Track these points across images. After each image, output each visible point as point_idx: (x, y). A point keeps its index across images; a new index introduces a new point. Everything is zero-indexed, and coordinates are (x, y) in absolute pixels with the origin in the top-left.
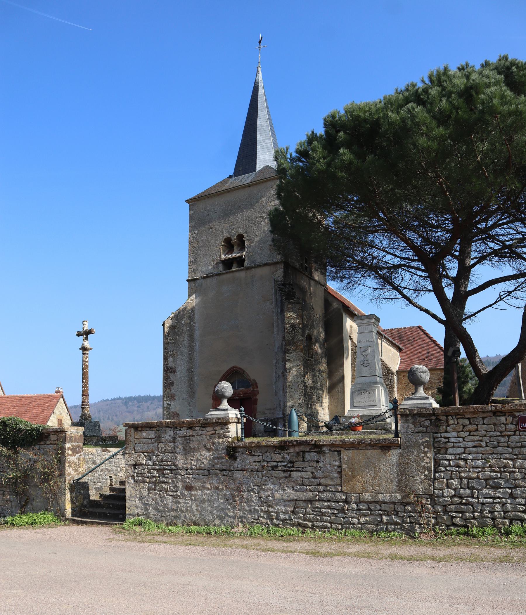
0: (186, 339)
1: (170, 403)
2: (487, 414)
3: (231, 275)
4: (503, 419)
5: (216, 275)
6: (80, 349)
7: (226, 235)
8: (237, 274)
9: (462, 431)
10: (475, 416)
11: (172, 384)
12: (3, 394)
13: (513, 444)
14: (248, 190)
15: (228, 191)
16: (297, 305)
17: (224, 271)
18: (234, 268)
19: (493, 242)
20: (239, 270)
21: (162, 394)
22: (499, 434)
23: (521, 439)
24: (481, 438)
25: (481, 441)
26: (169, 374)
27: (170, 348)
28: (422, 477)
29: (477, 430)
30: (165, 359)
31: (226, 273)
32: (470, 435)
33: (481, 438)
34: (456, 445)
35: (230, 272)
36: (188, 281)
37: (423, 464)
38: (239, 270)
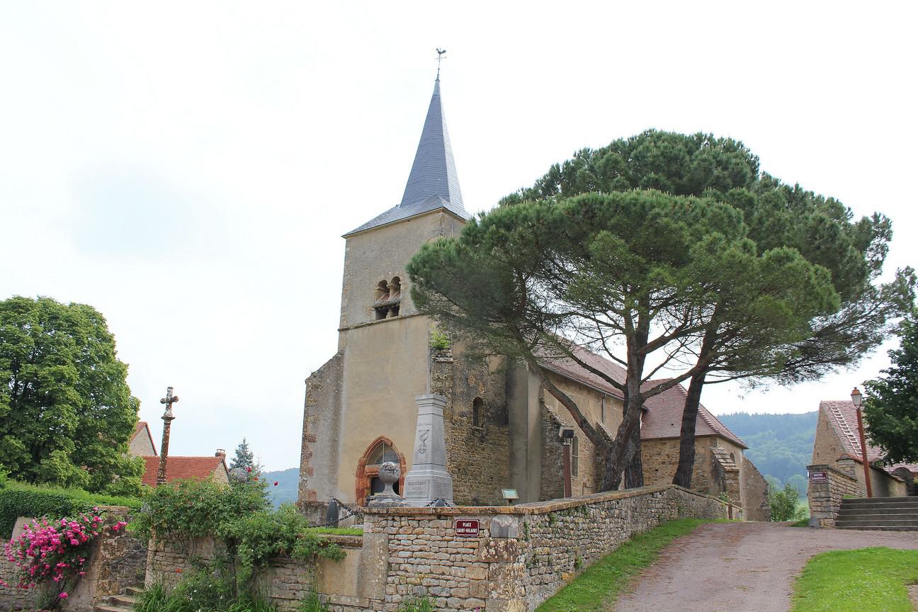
0: (331, 400)
1: (306, 479)
2: (433, 517)
3: (384, 324)
4: (443, 523)
5: (369, 325)
6: (162, 418)
7: (381, 278)
8: (391, 325)
9: (412, 534)
10: (422, 518)
11: (311, 455)
12: (153, 455)
13: (450, 550)
14: (407, 225)
15: (387, 226)
16: (448, 365)
17: (378, 321)
18: (388, 317)
19: (604, 312)
20: (393, 320)
21: (298, 466)
22: (440, 538)
23: (457, 544)
24: (425, 542)
25: (426, 545)
26: (307, 443)
27: (310, 412)
28: (377, 581)
29: (423, 533)
30: (305, 426)
31: (379, 323)
32: (417, 538)
33: (425, 542)
34: (405, 548)
35: (383, 322)
36: (338, 330)
37: (378, 566)
38: (393, 320)
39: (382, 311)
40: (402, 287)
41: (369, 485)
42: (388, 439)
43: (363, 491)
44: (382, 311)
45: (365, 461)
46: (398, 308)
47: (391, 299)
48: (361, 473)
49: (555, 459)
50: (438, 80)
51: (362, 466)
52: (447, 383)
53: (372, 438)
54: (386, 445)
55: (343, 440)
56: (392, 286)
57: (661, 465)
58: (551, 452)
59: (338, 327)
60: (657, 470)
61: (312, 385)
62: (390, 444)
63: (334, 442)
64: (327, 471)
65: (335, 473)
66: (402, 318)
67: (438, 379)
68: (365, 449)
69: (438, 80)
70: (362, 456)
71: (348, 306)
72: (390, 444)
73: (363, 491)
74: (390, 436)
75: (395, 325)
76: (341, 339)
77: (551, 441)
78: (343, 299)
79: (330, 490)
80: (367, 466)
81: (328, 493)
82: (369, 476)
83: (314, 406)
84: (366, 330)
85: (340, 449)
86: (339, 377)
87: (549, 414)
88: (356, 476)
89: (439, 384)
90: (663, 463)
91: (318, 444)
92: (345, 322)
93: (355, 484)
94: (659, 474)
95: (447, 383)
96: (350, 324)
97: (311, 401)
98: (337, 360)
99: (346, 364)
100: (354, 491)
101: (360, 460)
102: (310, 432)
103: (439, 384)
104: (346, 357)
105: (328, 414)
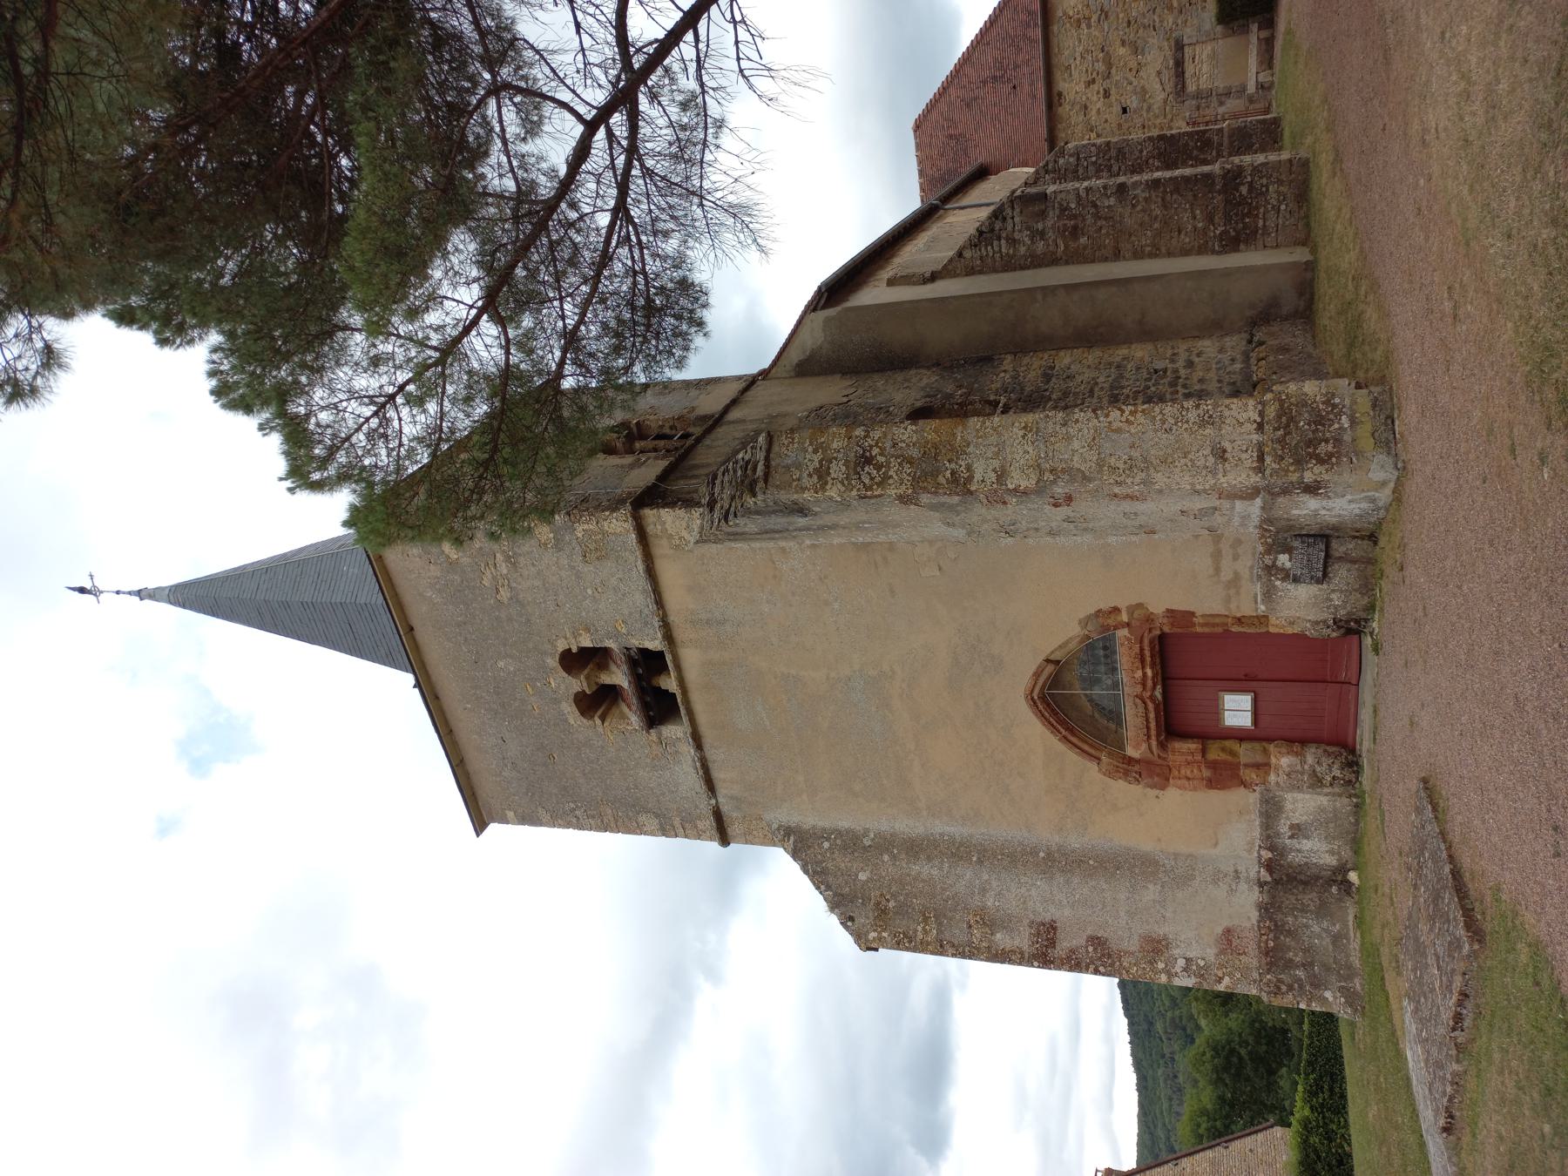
0: (923, 869)
1: (1181, 962)
16: (776, 448)
17: (685, 719)
18: (669, 683)
20: (678, 667)
39: (660, 708)
40: (587, 643)
41: (1192, 746)
42: (1037, 675)
43: (1213, 765)
44: (660, 708)
45: (1110, 755)
46: (644, 652)
47: (619, 677)
48: (1154, 773)
49: (1097, 217)
50: (141, 594)
51: (1128, 768)
52: (835, 445)
53: (1034, 732)
54: (1055, 681)
55: (1045, 835)
56: (587, 678)
57: (1113, 98)
58: (1075, 232)
59: (714, 846)
60: (1125, 110)
61: (874, 927)
62: (1050, 668)
63: (1054, 862)
64: (1151, 892)
65: (1156, 863)
66: (669, 637)
67: (822, 473)
68: (1072, 757)
69: (141, 594)
70: (1093, 766)
71: (657, 816)
72: (1050, 668)
73: (1213, 765)
74: (1022, 668)
75: (691, 658)
76: (749, 838)
77: (1042, 234)
78: (638, 830)
79: (1215, 881)
80: (1131, 752)
81: (1224, 887)
82: (1162, 745)
83: (940, 924)
84: (714, 754)
85: (1075, 842)
86: (851, 842)
87: (967, 254)
88: (1163, 788)
89: (838, 470)
90: (1107, 94)
91: (1062, 914)
92: (700, 825)
93: (1189, 795)
94: (1133, 102)
95: (835, 445)
96: (704, 805)
97: (925, 932)
98: (807, 848)
99: (810, 819)
100: (1216, 797)
101: (1109, 774)
102: (1022, 940)
103: (838, 470)
104: (794, 819)
105: (964, 879)
